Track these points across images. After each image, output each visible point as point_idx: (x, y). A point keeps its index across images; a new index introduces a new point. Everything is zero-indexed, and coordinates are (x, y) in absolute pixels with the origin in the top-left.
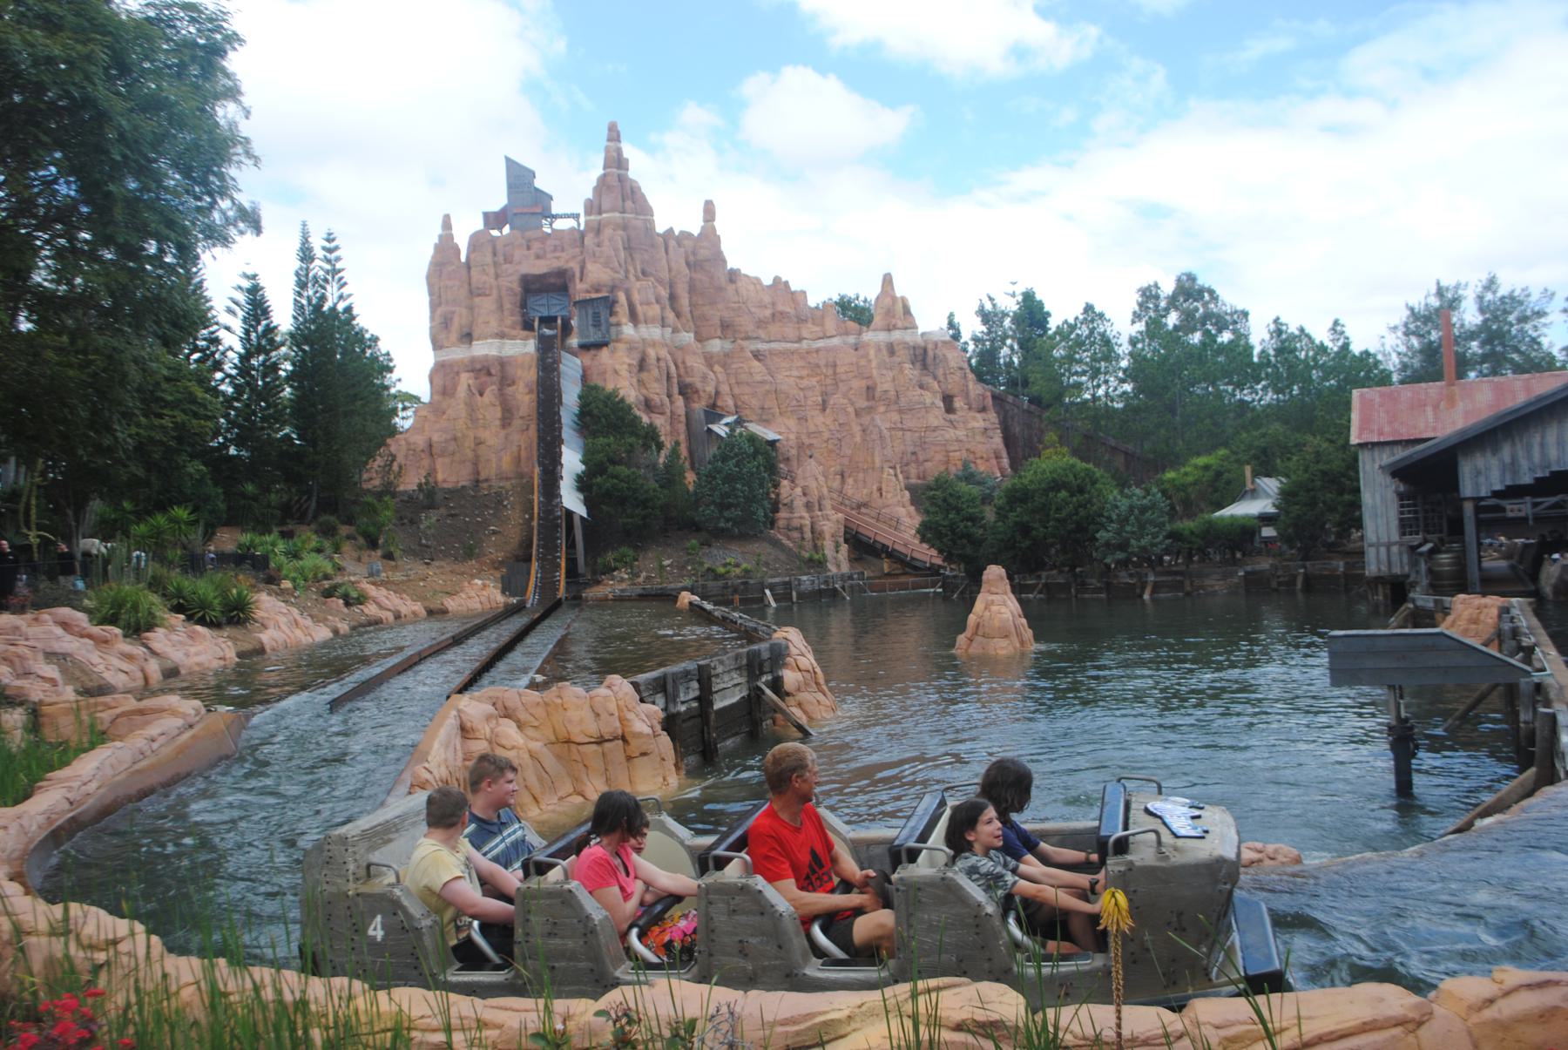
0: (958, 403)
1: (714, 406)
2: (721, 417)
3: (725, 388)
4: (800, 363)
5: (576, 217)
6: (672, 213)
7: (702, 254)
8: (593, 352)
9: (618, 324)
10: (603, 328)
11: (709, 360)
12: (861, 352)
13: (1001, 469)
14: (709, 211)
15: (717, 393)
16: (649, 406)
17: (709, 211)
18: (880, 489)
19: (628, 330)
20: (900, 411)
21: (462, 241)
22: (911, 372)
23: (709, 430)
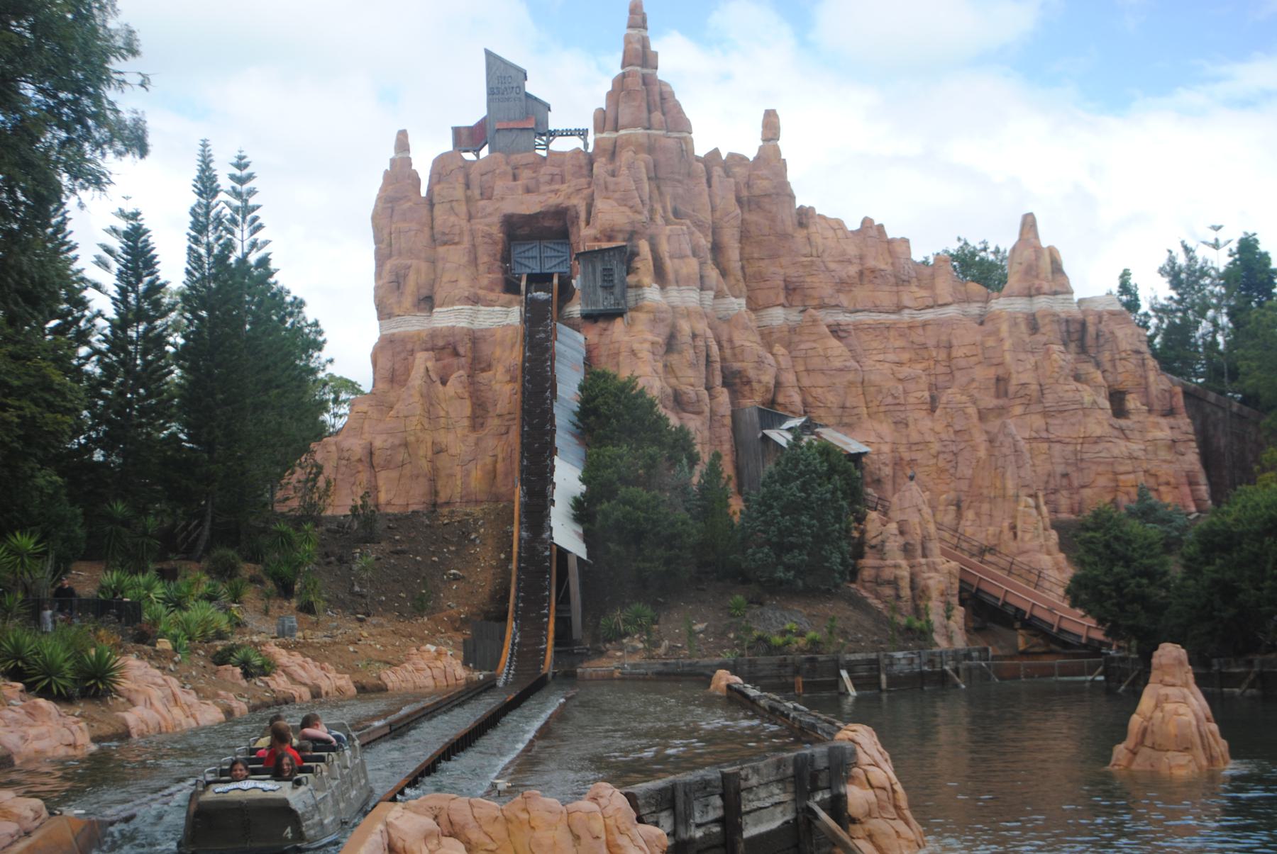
0: (1132, 402)
1: (773, 402)
2: (783, 419)
3: (789, 378)
4: (899, 343)
5: (582, 133)
6: (719, 126)
7: (758, 186)
8: (601, 325)
9: (639, 286)
10: (617, 290)
11: (767, 336)
12: (988, 327)
13: (1198, 501)
14: (771, 125)
15: (778, 385)
16: (679, 402)
17: (771, 125)
18: (1013, 528)
19: (652, 294)
20: (1046, 414)
21: (422, 166)
22: (1061, 357)
23: (766, 438)
